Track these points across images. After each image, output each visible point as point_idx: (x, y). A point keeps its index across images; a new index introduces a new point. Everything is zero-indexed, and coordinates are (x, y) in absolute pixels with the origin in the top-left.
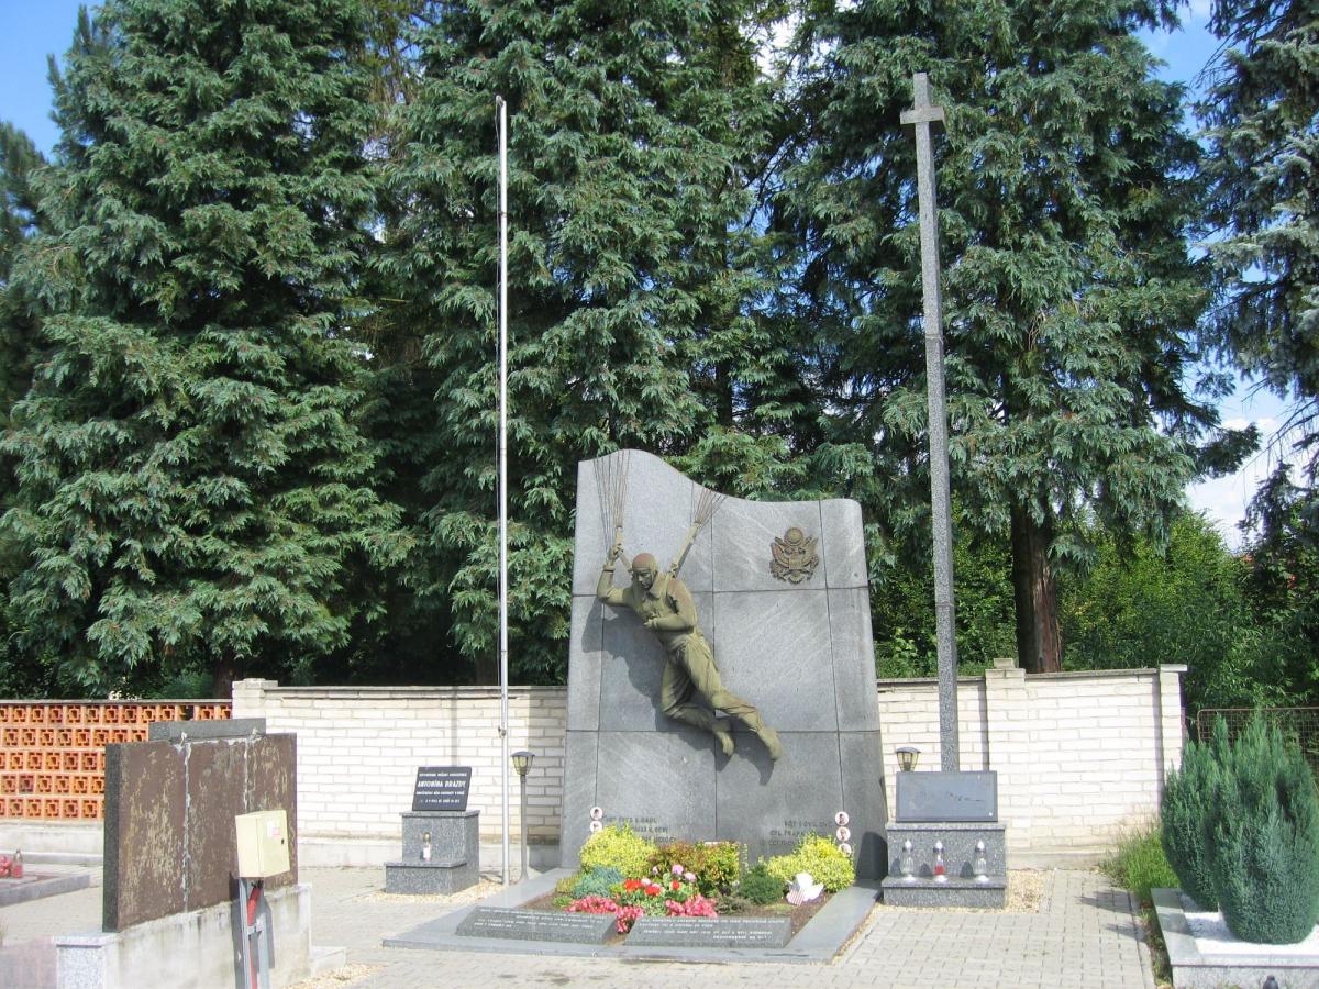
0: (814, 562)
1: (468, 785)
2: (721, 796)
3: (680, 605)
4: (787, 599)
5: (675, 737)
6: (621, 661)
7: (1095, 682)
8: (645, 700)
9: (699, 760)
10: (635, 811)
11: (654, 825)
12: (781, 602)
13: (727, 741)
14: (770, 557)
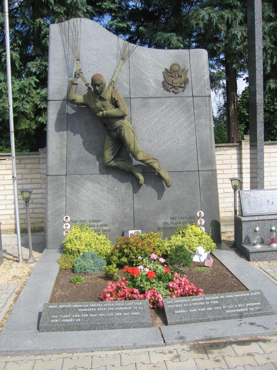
2: (136, 206)
3: (120, 103)
4: (171, 101)
5: (110, 177)
6: (78, 136)
7: (269, 146)
8: (92, 157)
10: (88, 217)
11: (99, 224)
13: (141, 177)
14: (162, 79)
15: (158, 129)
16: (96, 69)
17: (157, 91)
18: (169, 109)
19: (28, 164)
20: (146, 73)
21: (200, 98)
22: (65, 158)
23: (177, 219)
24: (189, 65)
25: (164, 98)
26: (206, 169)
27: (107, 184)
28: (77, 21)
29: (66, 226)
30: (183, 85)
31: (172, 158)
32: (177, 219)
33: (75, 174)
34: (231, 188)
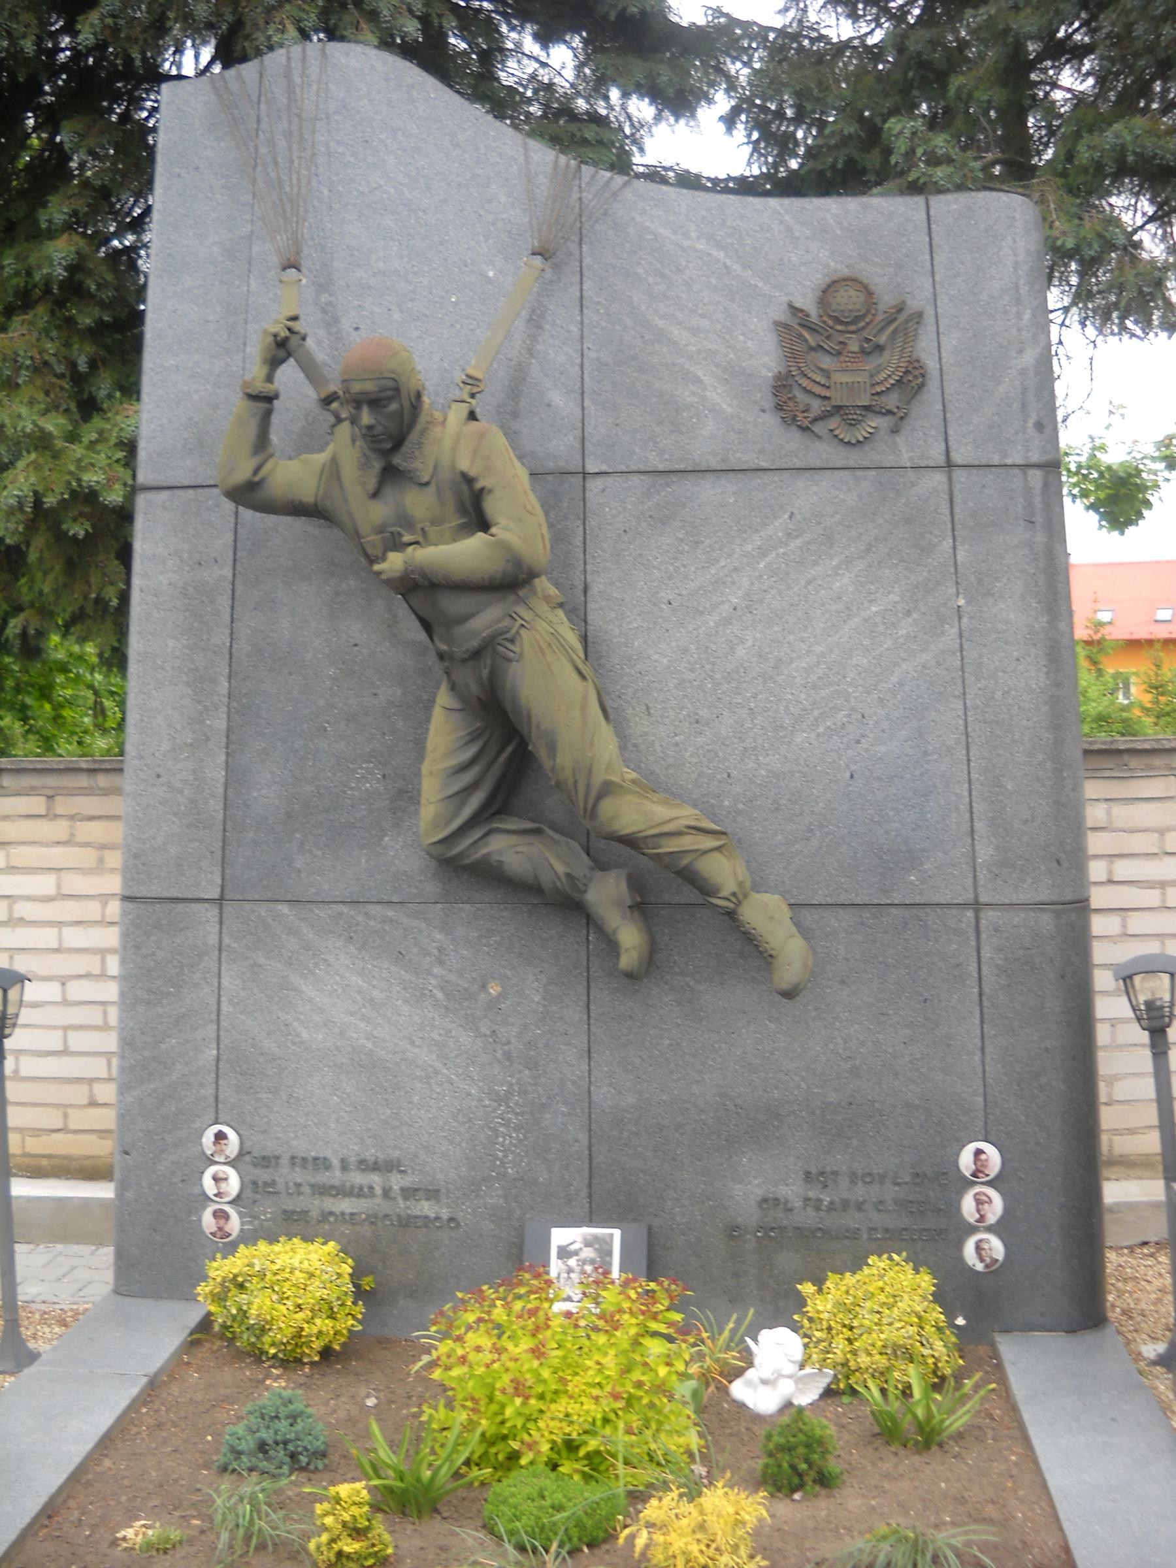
0: (912, 380)
2: (603, 1094)
9: (524, 985)
11: (396, 1182)
15: (741, 651)
16: (397, 316)
17: (740, 432)
18: (807, 537)
19: (91, 818)
20: (675, 332)
21: (989, 476)
22: (215, 806)
23: (844, 1182)
24: (928, 284)
25: (776, 477)
26: (1022, 898)
27: (441, 962)
28: (304, 59)
29: (216, 1179)
30: (892, 401)
31: (821, 826)
32: (844, 1182)
33: (270, 895)
34: (1143, 1045)
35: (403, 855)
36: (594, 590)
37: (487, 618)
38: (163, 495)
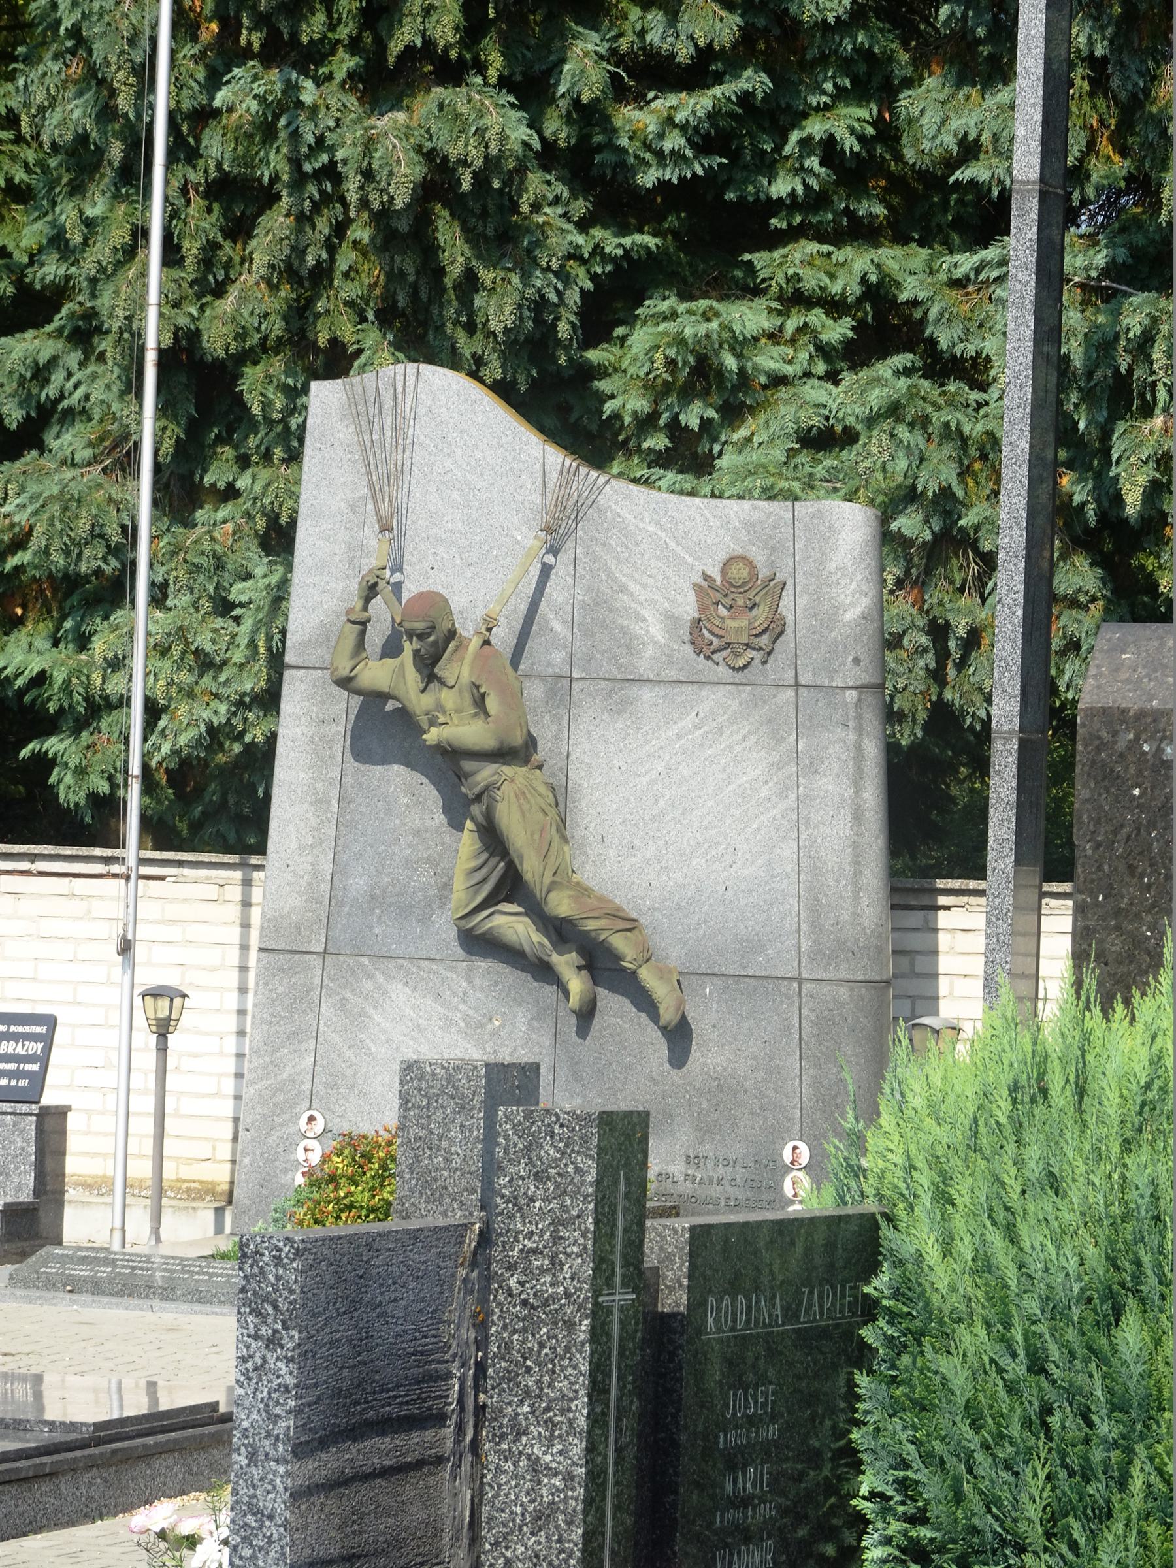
0: (776, 629)
1: (44, 1060)
12: (705, 707)
16: (458, 561)
18: (706, 728)
20: (632, 586)
23: (710, 1164)
24: (791, 563)
27: (464, 1002)
29: (306, 1150)
32: (710, 1164)
35: (444, 927)
36: (573, 757)
37: (486, 773)
38: (302, 672)
